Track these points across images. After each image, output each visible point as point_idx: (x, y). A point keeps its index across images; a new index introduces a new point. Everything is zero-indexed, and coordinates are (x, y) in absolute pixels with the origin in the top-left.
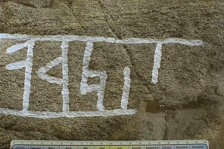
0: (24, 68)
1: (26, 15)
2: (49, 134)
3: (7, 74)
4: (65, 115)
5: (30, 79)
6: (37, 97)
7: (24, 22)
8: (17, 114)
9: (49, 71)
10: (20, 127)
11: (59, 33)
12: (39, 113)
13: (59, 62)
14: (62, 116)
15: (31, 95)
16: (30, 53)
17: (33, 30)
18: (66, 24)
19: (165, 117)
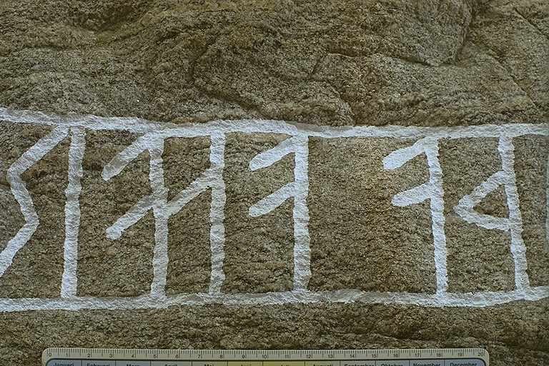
0: (428, 201)
1: (413, 83)
2: (492, 340)
3: (398, 216)
4: (521, 295)
5: (443, 223)
6: (463, 261)
7: (412, 98)
8: (426, 302)
9: (481, 203)
10: (434, 330)
11: (490, 121)
12: (469, 296)
13: (498, 184)
14: (517, 299)
15: (450, 258)
16: (434, 166)
17: (432, 115)
18: (503, 99)
19: (358, 280)
